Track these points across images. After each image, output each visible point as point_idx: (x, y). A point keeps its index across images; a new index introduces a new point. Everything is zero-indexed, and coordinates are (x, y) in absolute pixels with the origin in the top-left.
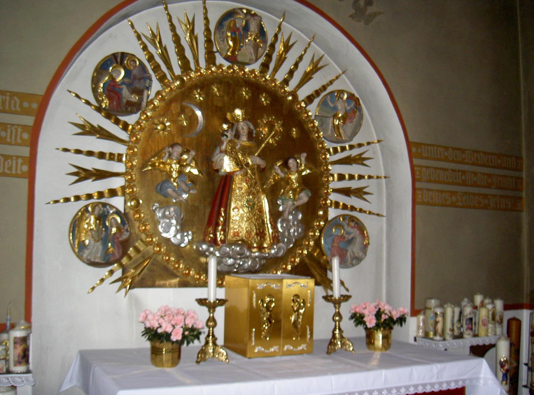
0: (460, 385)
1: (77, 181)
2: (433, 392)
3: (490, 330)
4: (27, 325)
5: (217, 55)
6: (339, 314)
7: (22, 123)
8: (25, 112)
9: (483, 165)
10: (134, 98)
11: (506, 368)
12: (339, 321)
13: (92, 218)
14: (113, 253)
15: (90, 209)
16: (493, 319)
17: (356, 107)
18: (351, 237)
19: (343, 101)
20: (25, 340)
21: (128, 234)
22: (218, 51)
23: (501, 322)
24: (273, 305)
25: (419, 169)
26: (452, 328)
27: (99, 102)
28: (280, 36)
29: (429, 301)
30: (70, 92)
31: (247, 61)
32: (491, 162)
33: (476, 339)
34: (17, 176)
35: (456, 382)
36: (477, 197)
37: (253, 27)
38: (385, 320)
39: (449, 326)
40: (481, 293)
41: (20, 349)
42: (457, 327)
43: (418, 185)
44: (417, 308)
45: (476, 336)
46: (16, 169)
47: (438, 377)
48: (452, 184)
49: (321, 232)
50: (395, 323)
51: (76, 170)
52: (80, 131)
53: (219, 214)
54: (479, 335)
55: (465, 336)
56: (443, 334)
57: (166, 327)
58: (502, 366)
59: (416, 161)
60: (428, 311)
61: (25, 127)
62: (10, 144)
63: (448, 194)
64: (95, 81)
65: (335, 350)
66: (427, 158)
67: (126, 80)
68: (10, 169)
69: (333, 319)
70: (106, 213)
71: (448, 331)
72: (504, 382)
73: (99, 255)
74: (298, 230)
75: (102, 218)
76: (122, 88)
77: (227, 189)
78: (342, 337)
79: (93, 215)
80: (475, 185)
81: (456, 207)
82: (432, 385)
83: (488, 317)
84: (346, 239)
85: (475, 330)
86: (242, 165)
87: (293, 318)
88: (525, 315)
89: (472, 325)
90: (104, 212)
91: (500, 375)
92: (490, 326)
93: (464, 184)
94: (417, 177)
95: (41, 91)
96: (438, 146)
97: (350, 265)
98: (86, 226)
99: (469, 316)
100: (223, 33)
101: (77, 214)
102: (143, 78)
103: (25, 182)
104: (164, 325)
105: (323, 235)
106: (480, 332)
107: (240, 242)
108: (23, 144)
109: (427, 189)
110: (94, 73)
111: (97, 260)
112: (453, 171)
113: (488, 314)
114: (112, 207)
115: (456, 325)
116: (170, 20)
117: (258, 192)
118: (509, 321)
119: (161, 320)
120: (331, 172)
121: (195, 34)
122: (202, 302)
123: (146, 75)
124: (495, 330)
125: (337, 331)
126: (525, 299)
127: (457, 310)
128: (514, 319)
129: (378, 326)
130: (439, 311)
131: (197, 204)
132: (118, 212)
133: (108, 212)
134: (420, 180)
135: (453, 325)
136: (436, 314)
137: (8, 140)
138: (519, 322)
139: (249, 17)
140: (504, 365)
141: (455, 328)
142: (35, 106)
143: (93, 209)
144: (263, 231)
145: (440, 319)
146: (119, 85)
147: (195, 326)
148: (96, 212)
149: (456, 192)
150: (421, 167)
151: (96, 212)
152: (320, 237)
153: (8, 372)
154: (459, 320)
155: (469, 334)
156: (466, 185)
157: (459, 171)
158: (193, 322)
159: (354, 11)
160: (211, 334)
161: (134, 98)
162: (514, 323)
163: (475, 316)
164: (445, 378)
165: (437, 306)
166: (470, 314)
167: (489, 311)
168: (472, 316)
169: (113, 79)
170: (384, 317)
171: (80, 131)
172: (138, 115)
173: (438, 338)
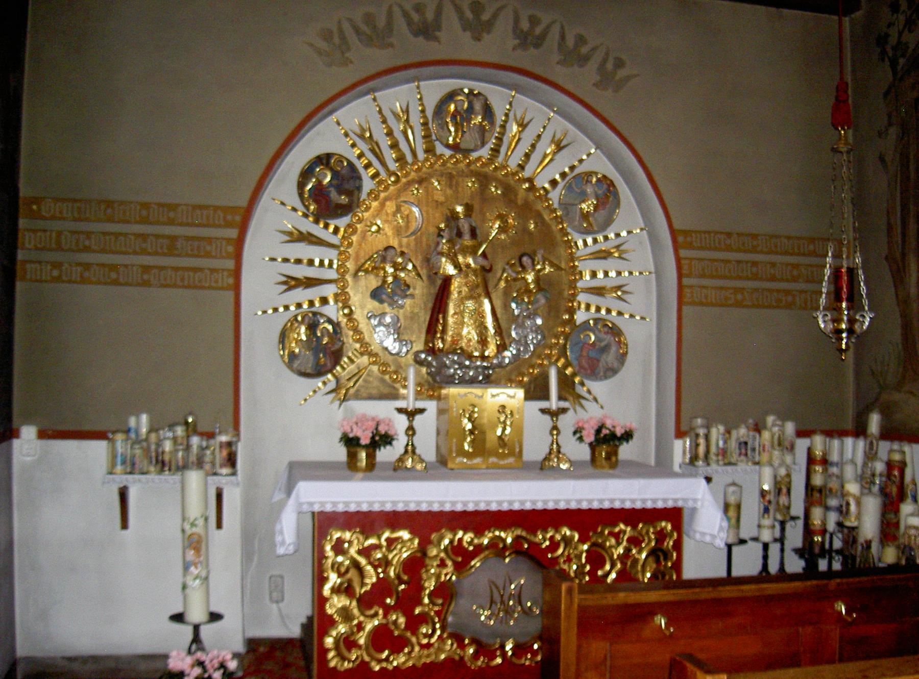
0: (670, 504)
1: (286, 291)
2: (633, 509)
4: (236, 433)
5: (437, 144)
6: (555, 428)
7: (226, 236)
8: (228, 225)
9: (786, 253)
10: (344, 199)
12: (557, 435)
13: (303, 329)
14: (325, 365)
15: (299, 318)
16: (780, 444)
17: (609, 191)
18: (603, 344)
19: (593, 185)
20: (229, 444)
21: (340, 344)
22: (437, 139)
23: (792, 448)
24: (476, 415)
25: (687, 262)
27: (307, 208)
28: (511, 115)
29: (694, 420)
30: (274, 199)
31: (472, 147)
32: (799, 249)
34: (222, 288)
36: (775, 294)
37: (478, 106)
38: (606, 435)
40: (773, 414)
41: (225, 453)
43: (686, 281)
46: (222, 282)
48: (739, 278)
49: (566, 339)
51: (284, 279)
52: (288, 238)
53: (438, 320)
57: (357, 432)
59: (683, 253)
61: (229, 240)
62: (215, 257)
63: (731, 291)
64: (301, 186)
66: (700, 248)
67: (334, 182)
68: (216, 281)
70: (316, 322)
73: (310, 366)
74: (536, 338)
75: (312, 327)
76: (330, 192)
77: (446, 293)
79: (304, 324)
80: (773, 279)
81: (743, 307)
84: (597, 347)
86: (460, 267)
87: (499, 432)
90: (314, 321)
93: (756, 277)
94: (684, 272)
95: (243, 202)
96: (716, 233)
97: (603, 378)
98: (296, 336)
100: (442, 119)
101: (286, 325)
102: (352, 178)
103: (231, 295)
104: (355, 429)
105: (569, 343)
107: (459, 351)
108: (228, 257)
109: (699, 287)
110: (299, 178)
111: (309, 371)
112: (739, 262)
114: (322, 315)
116: (380, 112)
117: (479, 296)
119: (355, 427)
120: (579, 269)
121: (375, 139)
122: (400, 411)
123: (355, 175)
131: (416, 310)
132: (330, 321)
133: (319, 322)
134: (689, 276)
136: (697, 435)
137: (214, 254)
139: (471, 97)
142: (238, 218)
143: (303, 318)
144: (486, 339)
145: (702, 441)
146: (327, 188)
147: (389, 432)
148: (307, 320)
149: (743, 289)
150: (691, 259)
151: (307, 320)
152: (565, 345)
153: (215, 474)
156: (761, 279)
157: (747, 262)
158: (387, 428)
159: (598, 78)
160: (410, 444)
161: (344, 199)
165: (702, 426)
169: (319, 183)
170: (605, 432)
171: (288, 238)
172: (350, 216)
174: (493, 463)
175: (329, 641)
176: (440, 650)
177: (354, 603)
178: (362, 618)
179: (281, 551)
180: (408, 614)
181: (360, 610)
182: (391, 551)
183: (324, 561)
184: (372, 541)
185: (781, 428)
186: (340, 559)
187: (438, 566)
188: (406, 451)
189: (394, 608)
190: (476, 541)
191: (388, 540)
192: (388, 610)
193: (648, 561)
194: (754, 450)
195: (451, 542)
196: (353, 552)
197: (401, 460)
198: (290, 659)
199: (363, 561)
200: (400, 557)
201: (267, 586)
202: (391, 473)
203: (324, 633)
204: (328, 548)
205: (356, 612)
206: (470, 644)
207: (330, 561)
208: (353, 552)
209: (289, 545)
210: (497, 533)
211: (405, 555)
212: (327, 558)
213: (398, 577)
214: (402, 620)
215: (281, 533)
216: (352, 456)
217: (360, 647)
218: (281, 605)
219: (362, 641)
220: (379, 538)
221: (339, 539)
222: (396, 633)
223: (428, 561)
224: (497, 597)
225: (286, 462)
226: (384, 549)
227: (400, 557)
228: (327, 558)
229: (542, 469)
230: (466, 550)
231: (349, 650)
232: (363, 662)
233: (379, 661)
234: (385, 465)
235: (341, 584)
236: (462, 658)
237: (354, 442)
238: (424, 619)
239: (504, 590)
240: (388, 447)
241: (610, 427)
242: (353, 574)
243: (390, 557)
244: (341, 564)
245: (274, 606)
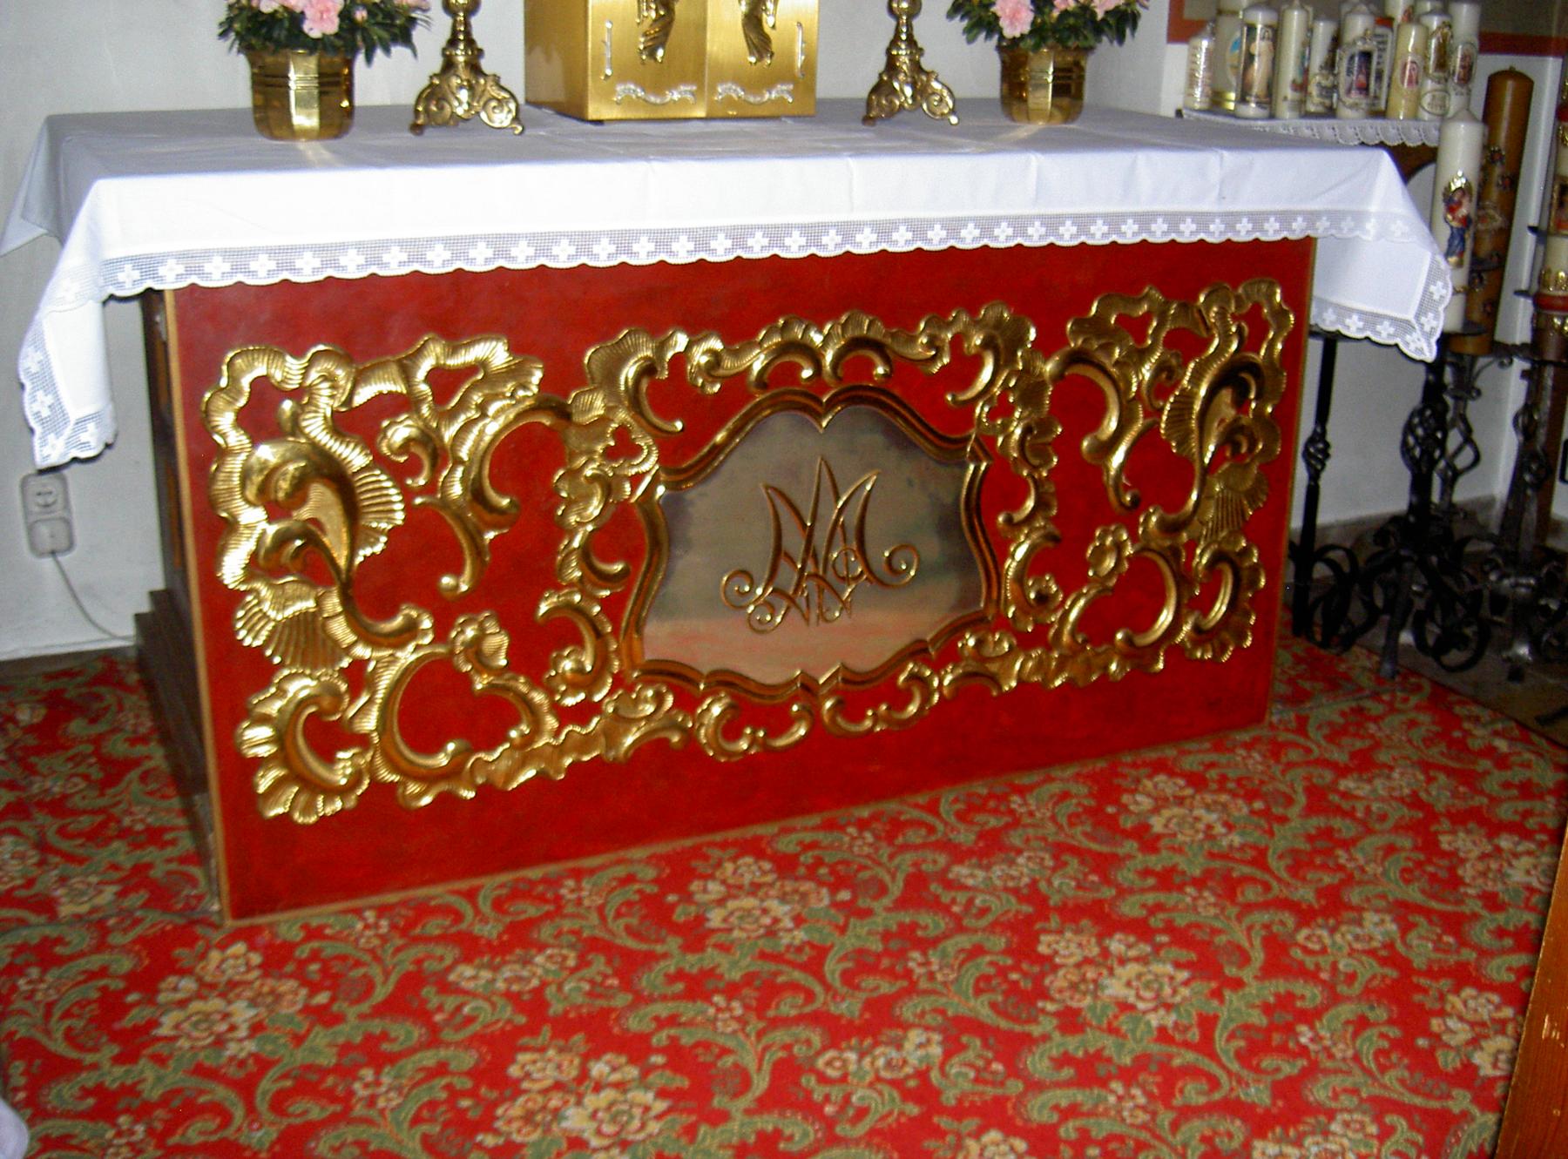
0: (1296, 231)
3: (1426, 100)
11: (1463, 211)
16: (1442, 64)
26: (1299, 80)
33: (1379, 123)
35: (1285, 217)
39: (1290, 71)
42: (1319, 84)
44: (1189, 13)
45: (1379, 114)
47: (1221, 197)
50: (1098, 28)
54: (1390, 112)
55: (1345, 112)
56: (1269, 99)
58: (1452, 206)
60: (1226, 24)
65: (892, 112)
69: (891, 10)
71: (1287, 91)
72: (1453, 259)
78: (917, 67)
82: (1202, 219)
83: (1426, 58)
85: (1376, 97)
88: (1547, 73)
89: (1368, 76)
91: (1445, 232)
92: (1429, 85)
99: (1360, 46)
106: (1392, 103)
113: (1427, 47)
115: (1317, 79)
118: (1495, 81)
124: (1444, 99)
125: (903, 53)
126: (1555, 25)
127: (1323, 30)
128: (1511, 73)
129: (1039, 32)
130: (1260, 19)
135: (1305, 72)
138: (1526, 88)
140: (1460, 204)
141: (1313, 90)
145: (1260, 46)
154: (1330, 65)
155: (1354, 106)
162: (1509, 89)
163: (1382, 50)
164: (1246, 202)
166: (1363, 38)
167: (1428, 36)
168: (1370, 46)
173: (1252, 108)
174: (729, 102)
175: (257, 739)
176: (621, 721)
177: (333, 603)
178: (362, 651)
179: (51, 451)
180: (517, 622)
181: (354, 623)
182: (452, 415)
183: (214, 467)
184: (384, 384)
185: (1446, 19)
186: (268, 453)
187: (610, 454)
188: (449, 65)
189: (468, 605)
190: (728, 363)
191: (431, 378)
192: (446, 613)
193: (1216, 400)
194: (1379, 76)
195: (648, 370)
196: (315, 427)
197: (434, 94)
198: (118, 747)
199: (355, 457)
200: (482, 432)
201: (20, 515)
202: (408, 138)
203: (235, 712)
204: (225, 421)
205: (341, 630)
206: (712, 692)
207: (235, 465)
208: (315, 427)
209: (81, 422)
210: (798, 332)
211: (492, 427)
212: (223, 453)
213: (476, 493)
214: (498, 642)
215: (46, 381)
216: (269, 86)
217: (363, 741)
218: (64, 559)
219: (369, 723)
220: (407, 375)
221: (261, 384)
222: (480, 684)
223: (573, 439)
224: (794, 542)
225: (38, 123)
226: (425, 410)
227: (482, 432)
228: (223, 453)
229: (868, 120)
230: (700, 397)
231: (329, 758)
232: (376, 784)
233: (429, 778)
234: (384, 116)
235: (282, 540)
236: (690, 736)
237: (280, 34)
238: (563, 631)
239: (814, 518)
240: (398, 51)
241: (302, 145)
242: (320, 503)
243: (448, 434)
244: (271, 473)
245: (48, 563)
